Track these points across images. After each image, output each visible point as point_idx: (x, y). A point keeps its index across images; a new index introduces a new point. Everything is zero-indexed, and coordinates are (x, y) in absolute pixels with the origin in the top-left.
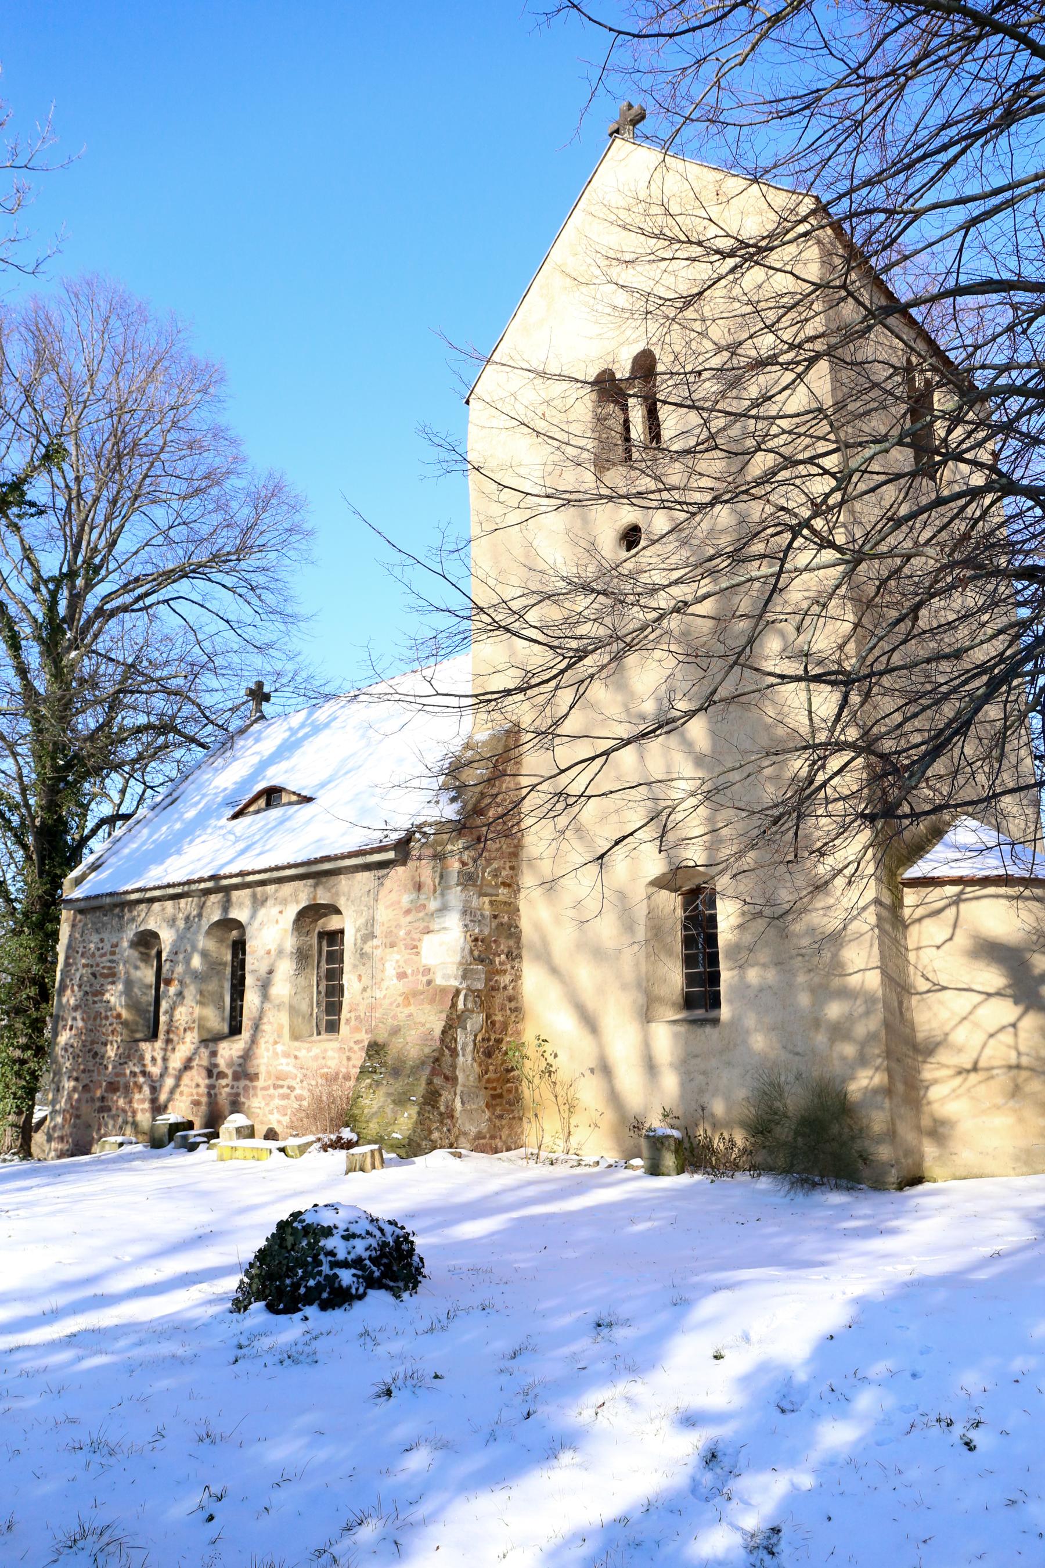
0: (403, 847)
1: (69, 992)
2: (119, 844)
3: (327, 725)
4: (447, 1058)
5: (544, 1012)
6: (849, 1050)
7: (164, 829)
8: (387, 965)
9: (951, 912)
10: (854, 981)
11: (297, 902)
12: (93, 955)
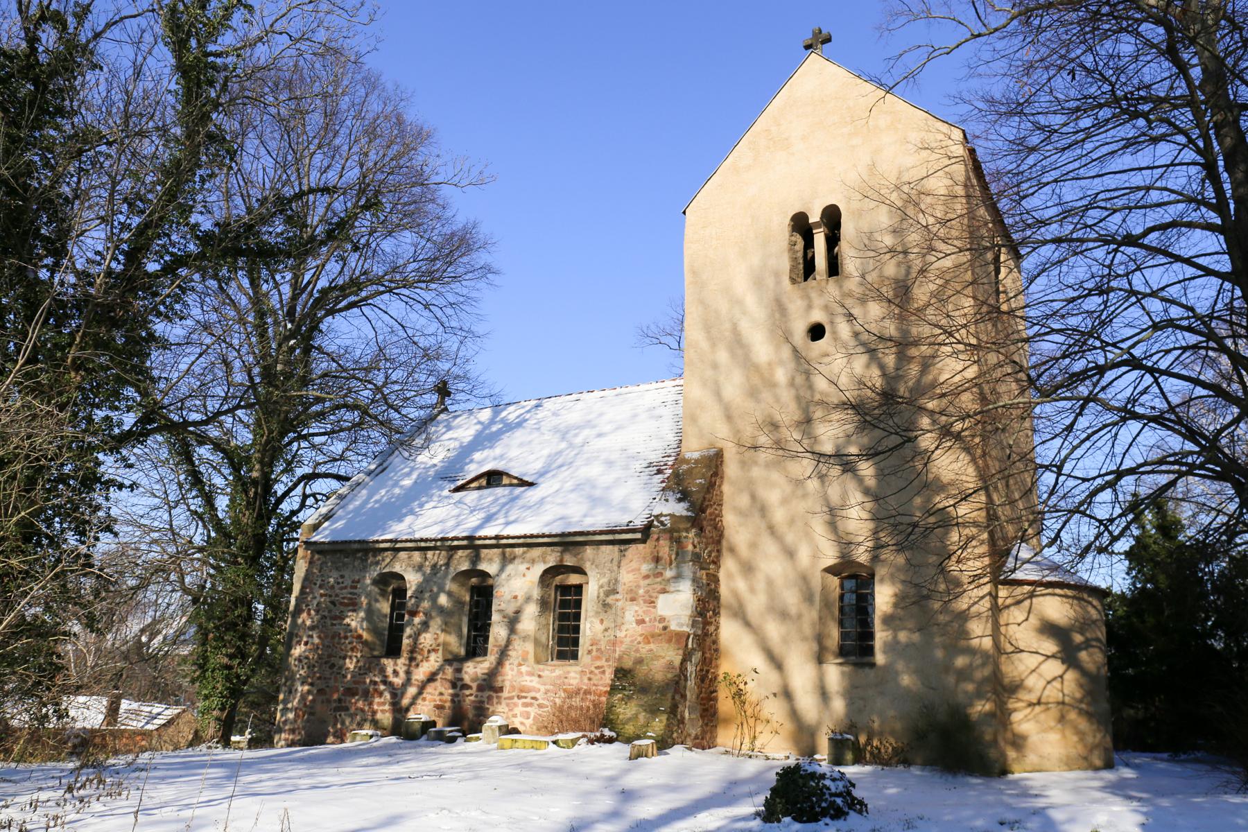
0: (646, 530)
1: (304, 615)
2: (345, 501)
3: (520, 424)
4: (682, 682)
5: (740, 654)
6: (970, 687)
7: (383, 492)
8: (627, 614)
9: (1027, 603)
10: (975, 642)
11: (545, 562)
12: (332, 587)
